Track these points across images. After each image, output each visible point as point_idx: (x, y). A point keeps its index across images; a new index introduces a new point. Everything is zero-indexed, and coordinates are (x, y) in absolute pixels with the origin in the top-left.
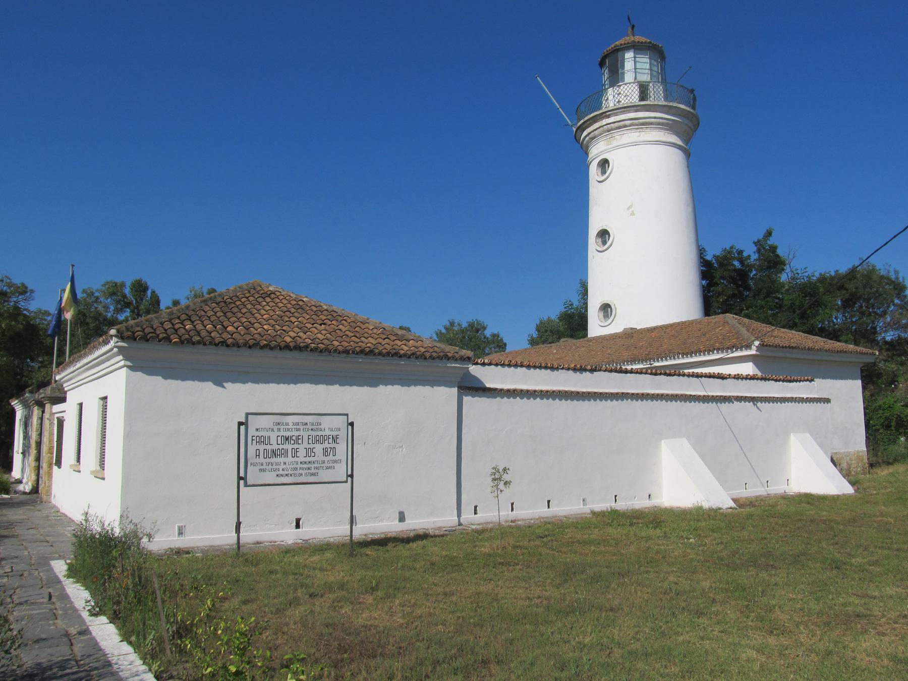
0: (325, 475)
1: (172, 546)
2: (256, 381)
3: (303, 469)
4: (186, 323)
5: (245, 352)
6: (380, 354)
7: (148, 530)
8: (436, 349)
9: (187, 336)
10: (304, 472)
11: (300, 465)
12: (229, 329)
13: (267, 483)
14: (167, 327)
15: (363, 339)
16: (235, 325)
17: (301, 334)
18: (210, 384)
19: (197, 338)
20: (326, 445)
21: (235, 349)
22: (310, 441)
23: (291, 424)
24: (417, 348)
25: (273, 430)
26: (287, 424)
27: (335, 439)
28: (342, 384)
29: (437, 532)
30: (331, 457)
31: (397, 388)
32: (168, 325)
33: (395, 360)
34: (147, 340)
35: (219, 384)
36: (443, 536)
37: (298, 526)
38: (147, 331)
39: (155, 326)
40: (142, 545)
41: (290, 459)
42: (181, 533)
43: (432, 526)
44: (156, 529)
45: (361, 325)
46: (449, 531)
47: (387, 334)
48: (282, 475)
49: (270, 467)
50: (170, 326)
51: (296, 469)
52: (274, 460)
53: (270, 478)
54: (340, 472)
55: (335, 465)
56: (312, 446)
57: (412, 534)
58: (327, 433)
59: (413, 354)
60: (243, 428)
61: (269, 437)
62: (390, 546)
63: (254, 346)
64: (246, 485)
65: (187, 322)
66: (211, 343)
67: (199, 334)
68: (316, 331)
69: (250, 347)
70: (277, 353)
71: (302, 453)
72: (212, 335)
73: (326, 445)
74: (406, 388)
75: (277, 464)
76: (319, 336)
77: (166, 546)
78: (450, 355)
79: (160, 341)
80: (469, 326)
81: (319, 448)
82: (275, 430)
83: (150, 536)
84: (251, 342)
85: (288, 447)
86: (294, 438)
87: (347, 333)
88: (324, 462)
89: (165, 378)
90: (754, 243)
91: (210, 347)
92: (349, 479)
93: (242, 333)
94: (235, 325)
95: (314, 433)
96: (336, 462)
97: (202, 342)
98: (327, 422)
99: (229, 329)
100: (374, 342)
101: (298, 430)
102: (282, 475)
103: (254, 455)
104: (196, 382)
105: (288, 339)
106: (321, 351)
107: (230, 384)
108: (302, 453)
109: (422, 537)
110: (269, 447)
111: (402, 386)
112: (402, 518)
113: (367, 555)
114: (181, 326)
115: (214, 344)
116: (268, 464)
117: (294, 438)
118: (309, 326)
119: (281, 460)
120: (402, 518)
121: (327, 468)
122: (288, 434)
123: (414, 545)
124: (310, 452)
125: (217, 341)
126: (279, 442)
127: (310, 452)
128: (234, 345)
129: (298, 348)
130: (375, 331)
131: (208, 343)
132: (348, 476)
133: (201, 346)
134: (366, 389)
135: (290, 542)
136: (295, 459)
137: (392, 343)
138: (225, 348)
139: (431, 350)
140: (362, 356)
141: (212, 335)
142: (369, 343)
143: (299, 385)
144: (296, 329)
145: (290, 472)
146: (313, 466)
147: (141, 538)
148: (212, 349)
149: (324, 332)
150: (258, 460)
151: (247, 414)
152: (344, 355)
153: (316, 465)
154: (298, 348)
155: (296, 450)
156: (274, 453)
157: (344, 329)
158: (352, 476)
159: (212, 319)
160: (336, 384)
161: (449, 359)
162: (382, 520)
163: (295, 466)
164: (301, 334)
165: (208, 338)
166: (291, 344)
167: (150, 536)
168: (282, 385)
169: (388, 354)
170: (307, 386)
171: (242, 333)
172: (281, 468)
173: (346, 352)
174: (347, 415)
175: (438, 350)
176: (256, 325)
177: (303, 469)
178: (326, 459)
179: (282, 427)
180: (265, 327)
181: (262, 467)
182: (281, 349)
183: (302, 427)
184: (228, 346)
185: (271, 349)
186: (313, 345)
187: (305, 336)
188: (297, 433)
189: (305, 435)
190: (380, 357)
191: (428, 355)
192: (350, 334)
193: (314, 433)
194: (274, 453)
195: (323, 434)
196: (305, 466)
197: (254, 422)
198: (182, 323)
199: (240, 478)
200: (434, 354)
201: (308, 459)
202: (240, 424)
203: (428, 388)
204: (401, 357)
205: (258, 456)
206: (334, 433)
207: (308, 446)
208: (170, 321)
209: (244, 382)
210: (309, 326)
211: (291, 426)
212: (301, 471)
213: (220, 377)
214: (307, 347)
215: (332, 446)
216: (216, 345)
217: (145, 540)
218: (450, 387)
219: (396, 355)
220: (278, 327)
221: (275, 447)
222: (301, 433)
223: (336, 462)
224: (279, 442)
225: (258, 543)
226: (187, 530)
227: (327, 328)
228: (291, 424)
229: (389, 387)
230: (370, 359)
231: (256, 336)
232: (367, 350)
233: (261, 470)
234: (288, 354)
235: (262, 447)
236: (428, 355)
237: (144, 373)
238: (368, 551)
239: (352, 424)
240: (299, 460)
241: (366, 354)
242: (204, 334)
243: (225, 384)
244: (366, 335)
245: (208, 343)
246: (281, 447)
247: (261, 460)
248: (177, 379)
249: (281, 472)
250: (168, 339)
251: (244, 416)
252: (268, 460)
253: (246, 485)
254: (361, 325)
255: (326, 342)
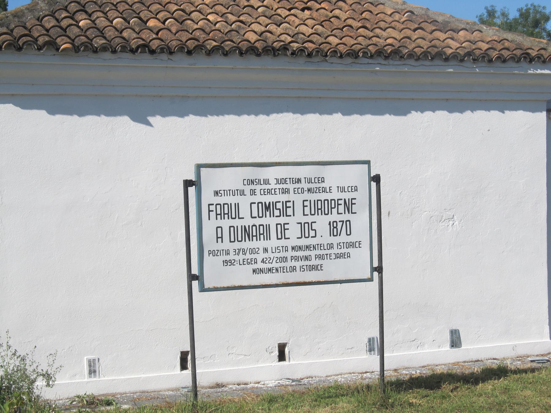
0: (333, 269)
1: (82, 393)
2: (202, 112)
3: (296, 259)
4: (80, 16)
5: (181, 61)
6: (411, 55)
7: (44, 367)
8: (507, 44)
9: (84, 39)
10: (298, 264)
11: (291, 253)
12: (152, 23)
13: (237, 284)
14: (48, 26)
15: (378, 31)
16: (161, 16)
17: (272, 27)
18: (126, 119)
19: (99, 42)
20: (334, 217)
21: (165, 56)
22: (307, 211)
23: (273, 182)
24: (474, 43)
25: (242, 193)
26: (266, 182)
27: (349, 206)
28: (347, 112)
29: (519, 365)
30: (343, 238)
31: (442, 114)
32: (49, 23)
33: (438, 67)
34: (20, 49)
35: (141, 118)
36: (533, 370)
37: (282, 357)
38: (18, 32)
39: (28, 25)
40: (36, 392)
41: (273, 242)
42: (92, 372)
43: (513, 354)
44: (55, 366)
45: (372, 8)
46: (539, 362)
47: (420, 21)
48: (261, 271)
49: (241, 257)
50: (53, 22)
51: (284, 259)
52: (247, 244)
53: (242, 275)
54: (360, 262)
55: (350, 250)
56: (310, 219)
57: (477, 369)
58: (335, 195)
59: (469, 54)
60: (192, 190)
61: (237, 206)
62: (446, 388)
63: (194, 50)
64: (203, 289)
65: (80, 16)
66: (124, 49)
67: (102, 33)
68: (297, 21)
69: (189, 53)
70: (235, 61)
71: (293, 231)
72: (125, 34)
73: (334, 217)
74: (456, 115)
75: (253, 251)
76: (303, 28)
77: (73, 393)
78: (533, 53)
79: (40, 49)
80: (521, 15)
81: (322, 223)
82: (247, 192)
83: (48, 377)
84: (191, 44)
85: (271, 221)
86: (279, 206)
87: (350, 22)
88: (331, 246)
89: (52, 112)
90: (486, 8)
91: (124, 55)
92: (376, 274)
93: (174, 30)
94: (161, 16)
95: (314, 197)
96: (352, 245)
97: (109, 48)
98: (334, 177)
99: (152, 23)
100: (399, 36)
101: (286, 191)
102: (261, 271)
103: (219, 234)
104: (103, 117)
105: (252, 37)
106: (310, 55)
107: (158, 118)
108: (293, 231)
109: (499, 372)
110: (237, 223)
111: (451, 111)
112: (455, 341)
113: (411, 405)
114: (71, 21)
115: (129, 49)
116: (238, 252)
117: (279, 206)
118: (284, 12)
119: (261, 244)
120: (455, 341)
121: (338, 256)
122: (268, 199)
123: (488, 386)
124: (307, 229)
125: (134, 44)
126: (255, 214)
127: (307, 229)
128: (162, 50)
129: (271, 51)
130: (397, 17)
131: (119, 48)
132: (374, 269)
133: (108, 55)
134: (388, 119)
135: (271, 384)
136: (283, 242)
137: (430, 37)
138: (147, 56)
139: (499, 46)
140: (381, 60)
141: (125, 34)
142: (389, 37)
143: (274, 116)
144: (262, 19)
145: (275, 265)
146: (313, 253)
147: (34, 381)
148: (126, 59)
149: (310, 22)
150: (220, 246)
151: (199, 167)
152: (349, 60)
153: (318, 252)
154: (271, 51)
155: (283, 228)
156: (247, 233)
157: (343, 16)
158: (379, 269)
159: (121, 8)
160: (336, 112)
161: (531, 60)
162: (422, 345)
163: (282, 254)
164: (272, 27)
165: (118, 40)
166: (258, 45)
167: (48, 377)
168: (245, 117)
169: (425, 55)
170: (288, 117)
171: (174, 30)
172: (261, 256)
173: (353, 54)
174: (368, 163)
175: (512, 46)
176: (195, 15)
177: (296, 259)
178: (335, 240)
179: (258, 188)
180: (210, 17)
181: (228, 258)
182: (241, 54)
183: (291, 187)
184: (152, 52)
185: (226, 54)
186: (295, 45)
187: (279, 30)
188: (284, 198)
189: (298, 199)
190: (412, 62)
191: (494, 54)
192: (355, 24)
193: (314, 197)
194: (247, 233)
195: (329, 196)
196: (300, 254)
197: (212, 180)
198: (72, 18)
199: (192, 277)
200: (506, 53)
201: (304, 242)
202: (188, 184)
203: (495, 114)
204: (447, 59)
205: (219, 238)
206: (347, 196)
207: (304, 219)
208: (52, 15)
209: (182, 114)
210: (284, 12)
211: (273, 185)
212: (293, 263)
213: (141, 108)
214: (285, 48)
215: (345, 217)
216: (133, 51)
217: (40, 383)
218: (541, 112)
219: (438, 56)
220: (232, 18)
221: (248, 222)
222: (291, 197)
223: (352, 245)
224: (255, 214)
225: (218, 386)
226: (102, 366)
227: (315, 15)
228: (273, 182)
229: (428, 114)
230: (394, 66)
231: (198, 33)
232: (389, 49)
233: (226, 262)
234: (253, 62)
235: (226, 223)
236: (494, 54)
237: (16, 105)
238: (412, 397)
239: (377, 179)
240: (289, 243)
241: (386, 58)
242: (110, 33)
243: (151, 119)
244: (382, 24)
245: (119, 48)
246: (258, 222)
247: (226, 245)
248: (70, 113)
249: (260, 265)
250: (52, 45)
251: (193, 169)
252: (237, 245)
253: (203, 289)
254: (372, 8)
255: (315, 38)
